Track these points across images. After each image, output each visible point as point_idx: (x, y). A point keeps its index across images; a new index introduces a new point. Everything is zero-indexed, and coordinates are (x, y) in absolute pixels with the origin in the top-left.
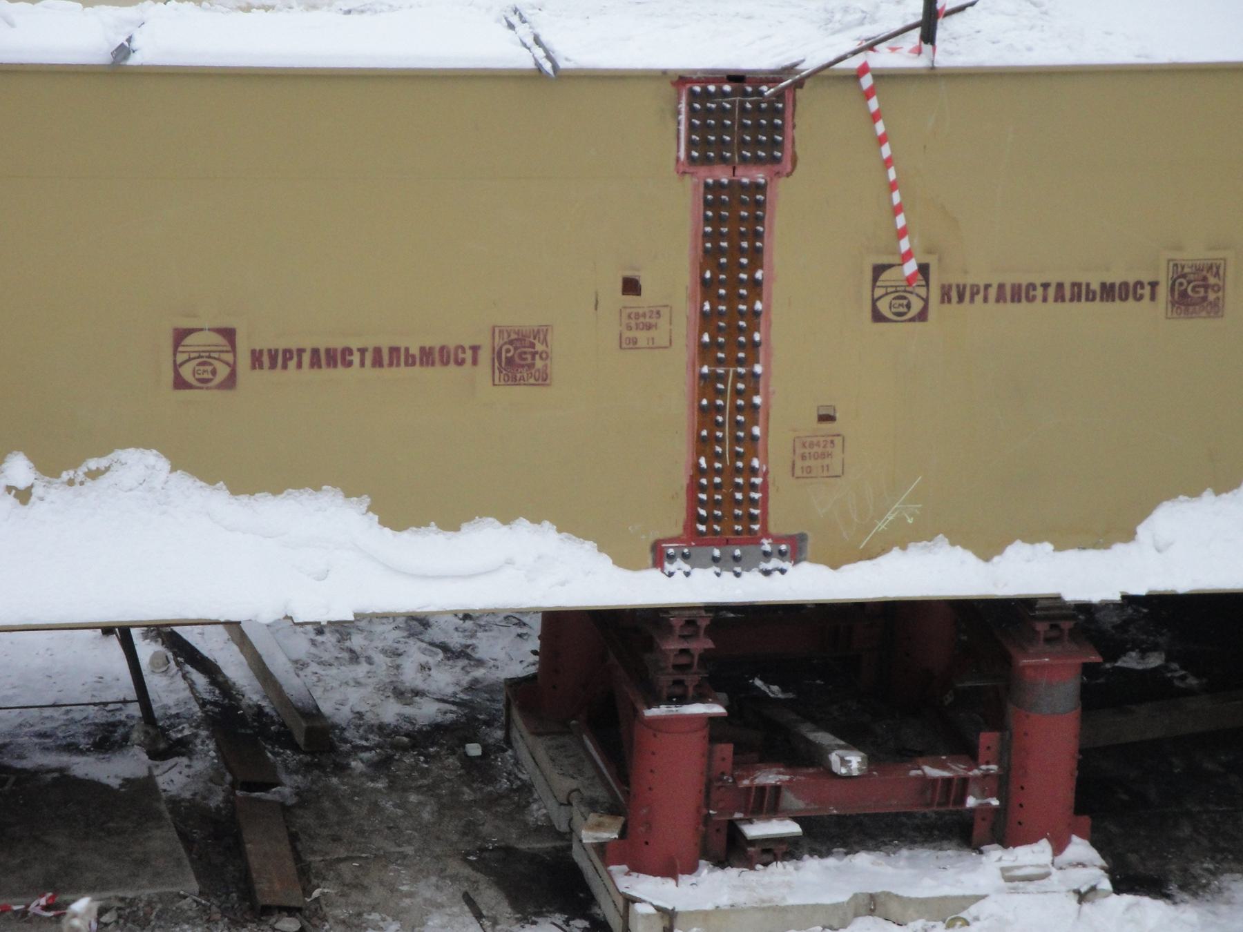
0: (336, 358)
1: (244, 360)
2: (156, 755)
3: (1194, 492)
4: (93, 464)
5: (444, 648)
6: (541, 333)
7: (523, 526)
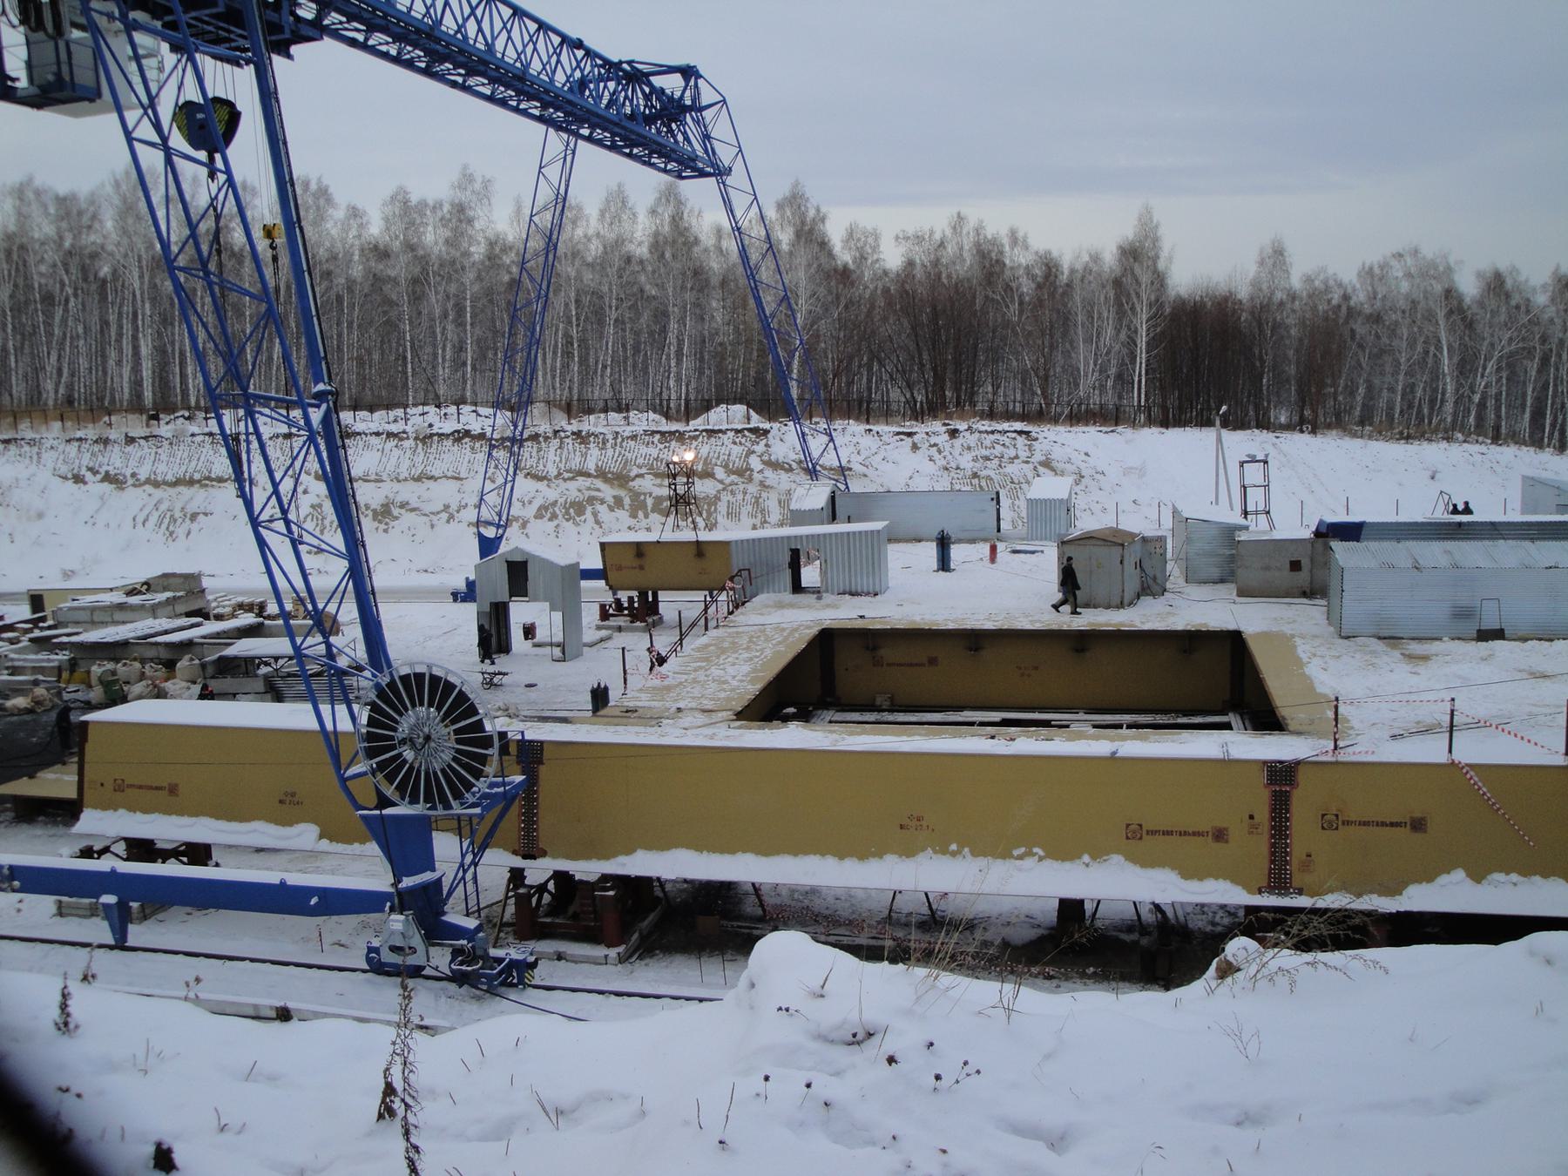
0: (1169, 833)
1: (1340, 823)
2: (1142, 935)
3: (1420, 882)
4: (1105, 858)
5: (1229, 912)
6: (1226, 829)
7: (1221, 880)
